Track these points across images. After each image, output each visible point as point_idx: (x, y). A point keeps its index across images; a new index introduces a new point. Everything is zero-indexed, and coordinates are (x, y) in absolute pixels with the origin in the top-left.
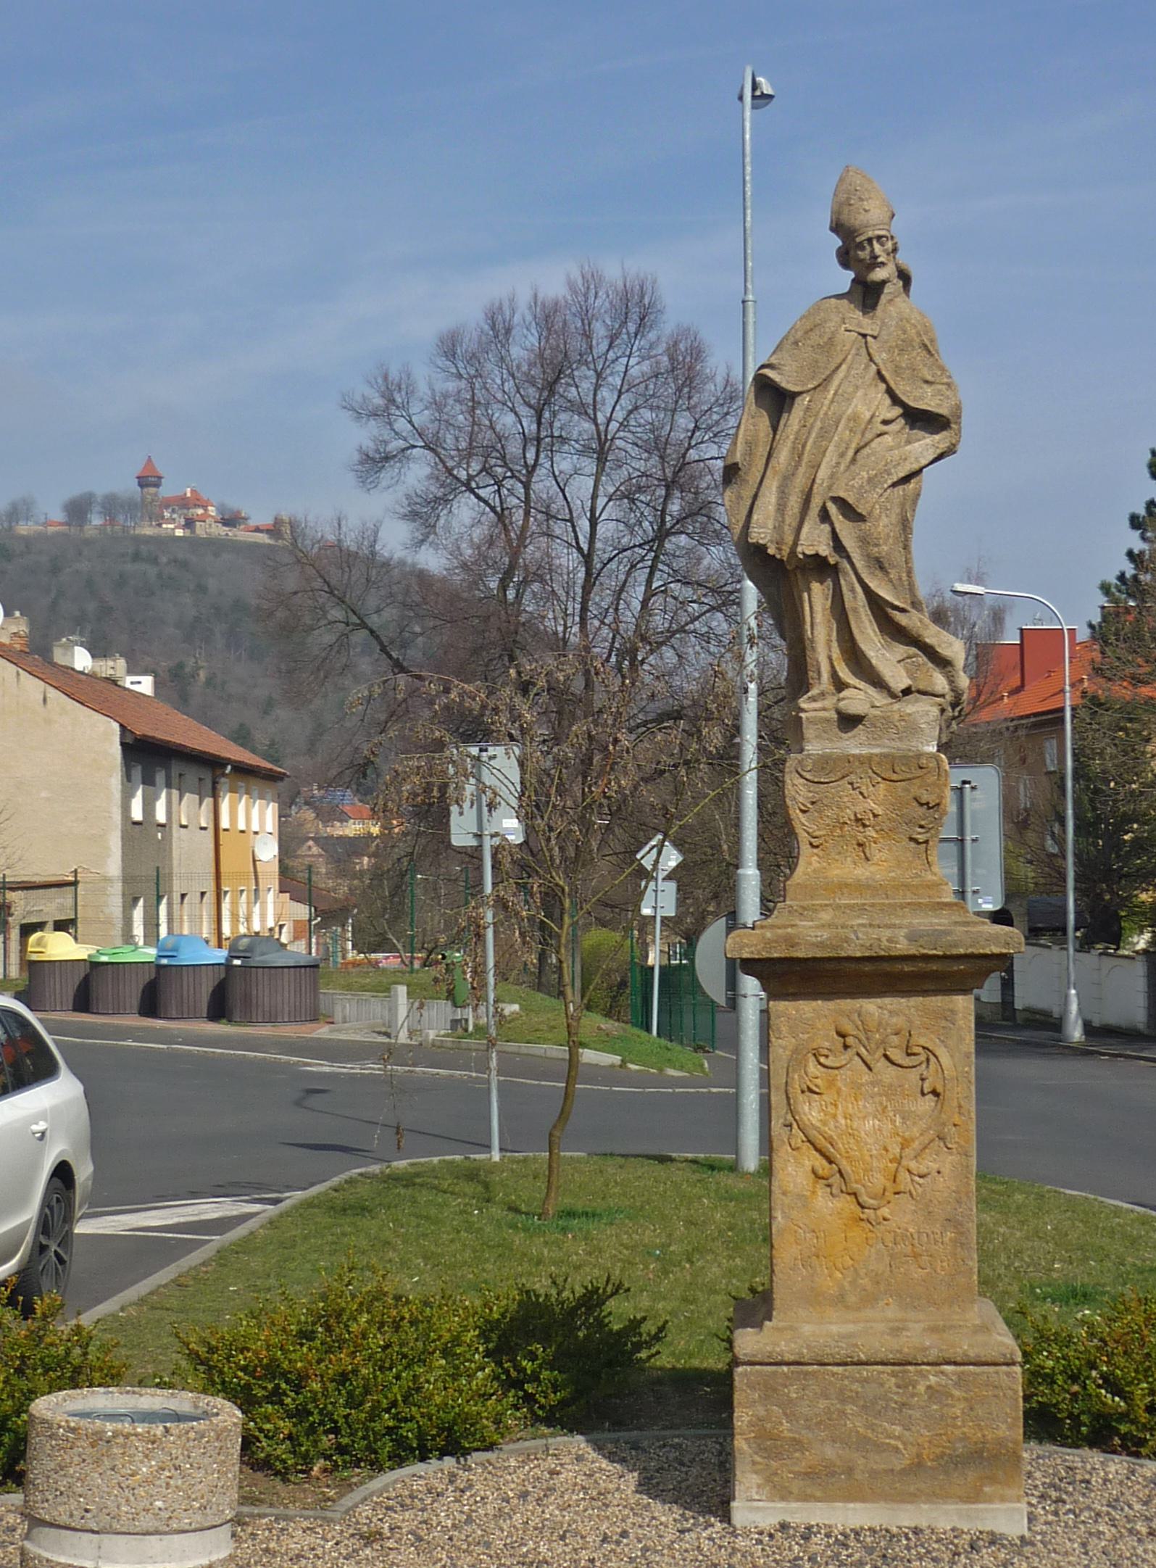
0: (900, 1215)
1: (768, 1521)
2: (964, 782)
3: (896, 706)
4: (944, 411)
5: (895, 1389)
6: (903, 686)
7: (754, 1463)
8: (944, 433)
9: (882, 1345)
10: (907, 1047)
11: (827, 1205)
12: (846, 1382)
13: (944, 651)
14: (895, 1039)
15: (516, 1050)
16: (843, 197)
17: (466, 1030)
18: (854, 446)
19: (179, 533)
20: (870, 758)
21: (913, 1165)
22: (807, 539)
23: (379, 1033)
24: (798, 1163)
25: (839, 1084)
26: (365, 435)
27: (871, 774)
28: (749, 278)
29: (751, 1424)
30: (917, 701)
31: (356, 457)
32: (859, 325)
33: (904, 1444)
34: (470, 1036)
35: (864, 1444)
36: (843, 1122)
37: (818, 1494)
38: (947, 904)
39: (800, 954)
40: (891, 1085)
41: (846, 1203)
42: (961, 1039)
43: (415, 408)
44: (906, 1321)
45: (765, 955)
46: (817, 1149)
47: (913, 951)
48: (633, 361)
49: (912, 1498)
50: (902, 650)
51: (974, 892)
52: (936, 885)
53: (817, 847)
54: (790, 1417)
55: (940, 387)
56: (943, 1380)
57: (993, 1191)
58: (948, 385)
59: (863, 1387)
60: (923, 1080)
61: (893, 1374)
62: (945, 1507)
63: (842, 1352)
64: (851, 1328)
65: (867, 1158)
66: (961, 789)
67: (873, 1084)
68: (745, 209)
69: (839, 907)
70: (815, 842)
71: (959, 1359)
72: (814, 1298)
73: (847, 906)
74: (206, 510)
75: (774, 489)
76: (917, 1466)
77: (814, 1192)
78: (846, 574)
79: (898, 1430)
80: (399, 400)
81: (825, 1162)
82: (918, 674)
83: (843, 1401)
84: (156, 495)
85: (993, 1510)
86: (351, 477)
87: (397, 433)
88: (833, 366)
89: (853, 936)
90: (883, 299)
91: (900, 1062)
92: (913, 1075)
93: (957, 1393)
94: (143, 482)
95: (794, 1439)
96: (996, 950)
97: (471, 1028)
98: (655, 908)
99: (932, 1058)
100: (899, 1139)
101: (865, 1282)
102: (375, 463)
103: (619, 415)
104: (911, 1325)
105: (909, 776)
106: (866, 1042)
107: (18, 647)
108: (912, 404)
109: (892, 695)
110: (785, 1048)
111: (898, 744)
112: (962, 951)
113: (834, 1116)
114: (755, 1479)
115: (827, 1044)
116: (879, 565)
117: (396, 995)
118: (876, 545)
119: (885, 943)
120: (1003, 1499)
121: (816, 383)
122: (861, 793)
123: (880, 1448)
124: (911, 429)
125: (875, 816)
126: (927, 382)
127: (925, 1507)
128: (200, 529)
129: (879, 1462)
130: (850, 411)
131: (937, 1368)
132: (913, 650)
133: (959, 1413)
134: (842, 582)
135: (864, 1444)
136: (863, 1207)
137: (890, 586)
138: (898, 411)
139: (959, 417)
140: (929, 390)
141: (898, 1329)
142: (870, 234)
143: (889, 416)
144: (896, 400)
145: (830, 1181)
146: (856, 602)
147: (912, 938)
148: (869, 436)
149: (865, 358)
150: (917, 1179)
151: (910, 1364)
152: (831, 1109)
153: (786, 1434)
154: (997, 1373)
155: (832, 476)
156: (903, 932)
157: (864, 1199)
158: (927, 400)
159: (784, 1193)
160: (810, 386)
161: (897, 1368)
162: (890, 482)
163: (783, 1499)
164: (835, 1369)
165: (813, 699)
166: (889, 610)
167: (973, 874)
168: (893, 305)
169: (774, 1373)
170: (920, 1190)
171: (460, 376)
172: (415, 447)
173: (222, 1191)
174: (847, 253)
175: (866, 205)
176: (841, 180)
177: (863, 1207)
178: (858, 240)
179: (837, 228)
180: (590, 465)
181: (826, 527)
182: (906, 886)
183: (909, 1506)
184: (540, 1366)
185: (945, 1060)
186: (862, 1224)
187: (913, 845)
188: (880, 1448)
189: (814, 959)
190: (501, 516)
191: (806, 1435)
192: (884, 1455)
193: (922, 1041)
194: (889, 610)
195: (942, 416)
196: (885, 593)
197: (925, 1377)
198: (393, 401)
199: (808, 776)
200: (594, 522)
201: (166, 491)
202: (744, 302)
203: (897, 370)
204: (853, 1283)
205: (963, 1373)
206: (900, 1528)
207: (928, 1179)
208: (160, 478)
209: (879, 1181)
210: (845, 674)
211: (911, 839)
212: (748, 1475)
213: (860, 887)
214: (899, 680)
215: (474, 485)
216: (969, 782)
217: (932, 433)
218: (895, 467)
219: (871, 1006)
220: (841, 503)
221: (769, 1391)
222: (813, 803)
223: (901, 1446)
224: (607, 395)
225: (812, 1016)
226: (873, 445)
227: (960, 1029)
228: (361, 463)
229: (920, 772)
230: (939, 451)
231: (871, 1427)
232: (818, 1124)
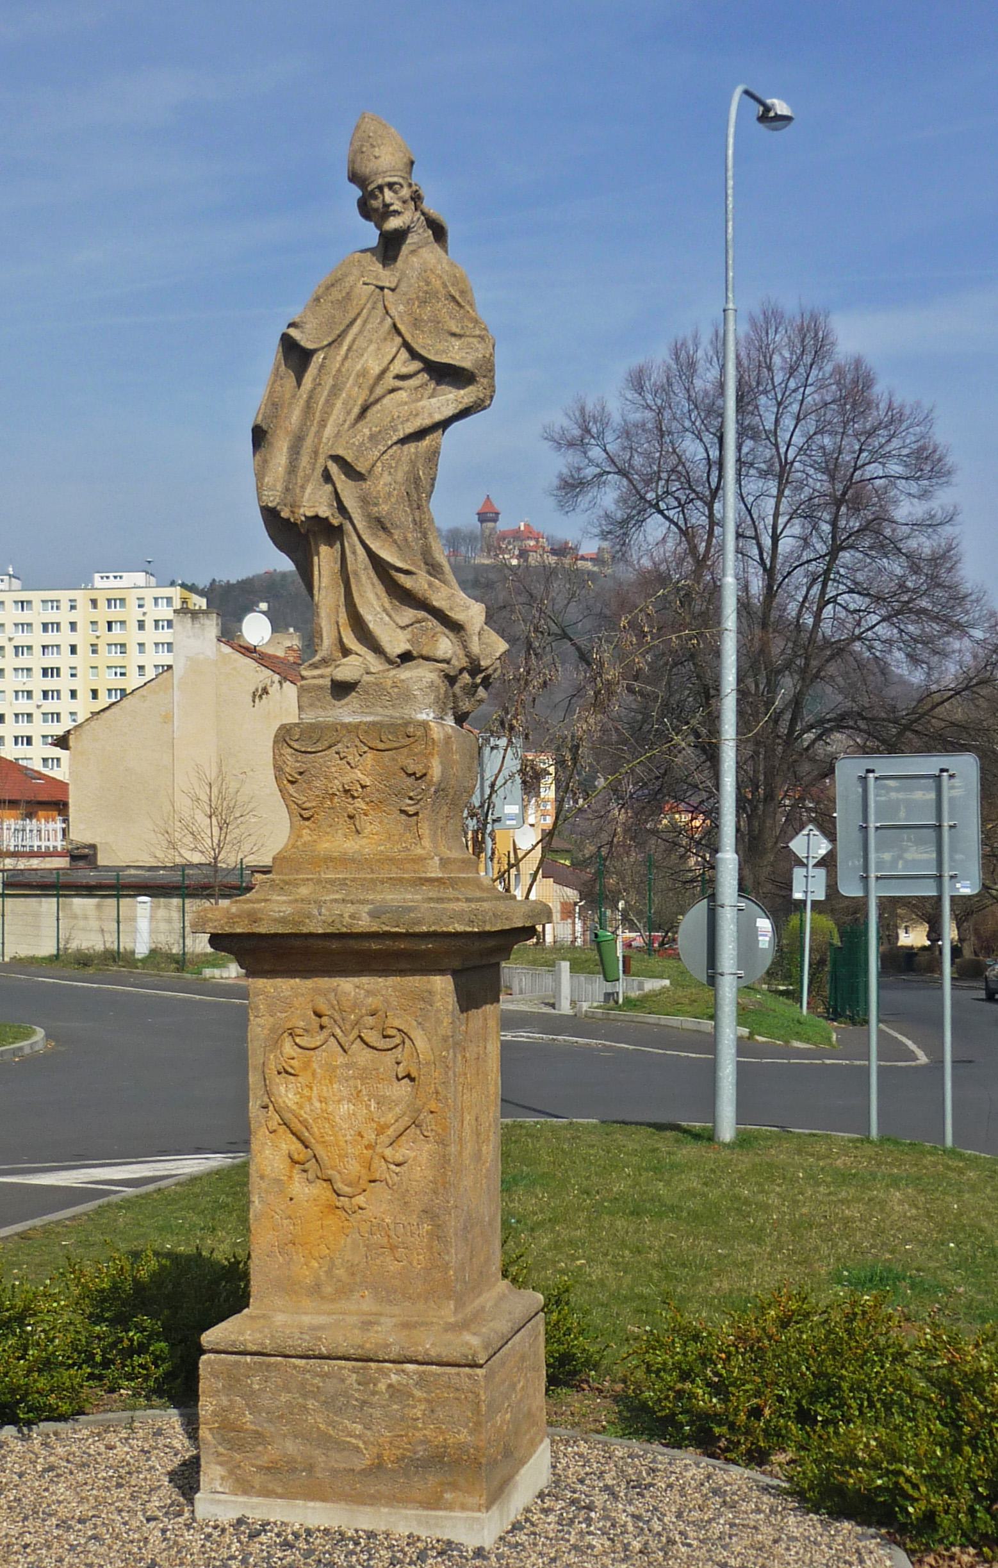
0: (377, 1205)
1: (227, 1515)
2: (942, 770)
3: (393, 673)
4: (467, 364)
5: (356, 1386)
6: (399, 651)
7: (219, 1455)
8: (471, 387)
9: (347, 1339)
10: (384, 1029)
11: (302, 1189)
12: (308, 1376)
13: (457, 616)
14: (370, 1021)
15: (656, 1021)
16: (357, 144)
17: (617, 1002)
18: (360, 402)
19: (514, 562)
20: (357, 726)
21: (388, 1152)
22: (309, 500)
23: (546, 1004)
24: (276, 1146)
25: (315, 1065)
26: (560, 463)
27: (359, 744)
28: (730, 287)
29: (215, 1414)
30: (418, 666)
31: (556, 482)
32: (377, 278)
33: (364, 1443)
34: (620, 1008)
35: (325, 1441)
36: (318, 1105)
37: (280, 1490)
38: (430, 880)
39: (262, 930)
40: (365, 1069)
41: (319, 1190)
42: (439, 1022)
43: (609, 437)
44: (381, 1315)
45: (228, 930)
46: (294, 1134)
47: (374, 929)
48: (809, 390)
49: (372, 1500)
50: (409, 614)
51: (952, 877)
52: (422, 859)
53: (308, 819)
54: (254, 1409)
55: (471, 340)
56: (404, 1379)
57: (948, 1168)
58: (482, 337)
59: (324, 1382)
60: (398, 1063)
61: (353, 1370)
62: (404, 1512)
63: (304, 1344)
64: (322, 1320)
65: (342, 1143)
66: (939, 776)
67: (348, 1066)
68: (727, 221)
69: (319, 881)
70: (306, 814)
71: (420, 1358)
72: (288, 1286)
73: (328, 881)
74: (537, 542)
75: (285, 450)
76: (377, 1468)
77: (290, 1177)
78: (349, 536)
79: (358, 1428)
80: (594, 430)
81: (300, 1146)
82: (424, 640)
83: (305, 1396)
84: (494, 528)
85: (451, 1518)
86: (551, 502)
87: (590, 461)
88: (347, 322)
89: (316, 912)
90: (405, 250)
91: (375, 1045)
92: (389, 1058)
93: (418, 1393)
94: (483, 517)
95: (256, 1432)
96: (460, 928)
97: (621, 1001)
98: (806, 892)
99: (407, 1040)
100: (375, 1126)
101: (340, 1272)
102: (572, 487)
103: (798, 440)
104: (383, 1320)
105: (396, 745)
106: (340, 1022)
107: (291, 659)
108: (432, 357)
109: (390, 661)
110: (262, 1027)
111: (391, 712)
112: (425, 929)
113: (310, 1099)
114: (219, 1471)
115: (302, 1024)
116: (381, 525)
117: (560, 970)
118: (376, 505)
119: (347, 920)
120: (463, 1507)
121: (330, 339)
122: (349, 763)
123: (342, 1447)
124: (438, 384)
125: (363, 787)
126: (454, 335)
127: (385, 1510)
128: (533, 559)
129: (338, 1460)
130: (359, 367)
131: (399, 1366)
132: (422, 614)
133: (419, 1414)
134: (346, 544)
135: (325, 1441)
136: (339, 1195)
137: (394, 549)
138: (416, 365)
139: (492, 370)
140: (457, 343)
141: (371, 1323)
142: (380, 181)
143: (404, 370)
144: (414, 355)
145: (307, 1166)
146: (359, 561)
147: (374, 915)
148: (379, 391)
149: (380, 311)
150: (393, 1167)
151: (371, 1360)
152: (306, 1092)
153: (249, 1426)
154: (458, 1374)
155: (338, 435)
156: (368, 908)
157: (339, 1185)
158: (456, 354)
159: (262, 1177)
160: (325, 343)
161: (360, 1364)
162: (395, 439)
163: (245, 1493)
164: (301, 1362)
165: (315, 666)
166: (393, 573)
167: (952, 859)
168: (420, 256)
169: (237, 1363)
170: (396, 1179)
171: (648, 407)
172: (609, 473)
173: (233, 1147)
174: (365, 204)
175: (377, 152)
176: (357, 127)
177: (339, 1195)
178: (369, 189)
179: (355, 178)
180: (772, 486)
181: (329, 487)
182: (391, 860)
183: (368, 1509)
184: (150, 1337)
185: (421, 1042)
186: (338, 1212)
187: (404, 817)
188: (342, 1447)
189: (276, 935)
190: (686, 533)
191: (268, 1428)
192: (346, 1453)
193: (397, 1023)
194: (393, 573)
195: (463, 369)
196: (388, 555)
197: (387, 1375)
198: (588, 431)
199: (296, 746)
200: (775, 539)
201: (503, 525)
202: (724, 311)
203: (416, 323)
204: (329, 1273)
205: (424, 1372)
206: (357, 1531)
207: (404, 1168)
209: (354, 1168)
210: (351, 641)
211: (402, 812)
212: (213, 1466)
213: (344, 860)
214: (396, 642)
215: (662, 506)
216: (947, 771)
217: (459, 388)
218: (402, 423)
219: (347, 985)
220: (337, 459)
221: (233, 1382)
222: (301, 773)
223: (361, 1445)
224: (788, 422)
225: (283, 996)
226: (385, 401)
227: (438, 1011)
228: (559, 488)
229: (407, 741)
230: (461, 407)
231: (331, 1424)
232: (294, 1107)
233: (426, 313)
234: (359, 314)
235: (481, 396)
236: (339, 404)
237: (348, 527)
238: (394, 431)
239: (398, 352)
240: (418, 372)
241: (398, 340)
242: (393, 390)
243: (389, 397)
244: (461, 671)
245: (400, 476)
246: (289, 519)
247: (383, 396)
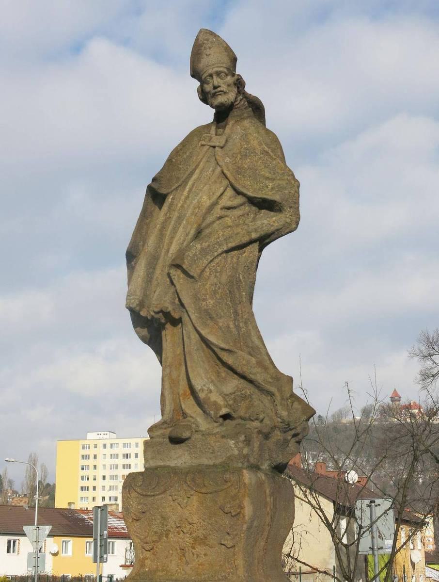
31: (419, 376)
116: (208, 315)
118: (204, 300)
138: (240, 200)
142: (210, 71)
143: (229, 204)
144: (238, 193)
148: (210, 219)
162: (220, 251)
181: (172, 289)
208: (400, 397)
226: (215, 225)
233: (247, 163)
234: (197, 166)
235: (288, 220)
236: (181, 229)
237: (185, 318)
238: (220, 246)
239: (225, 190)
240: (241, 205)
241: (225, 182)
242: (220, 218)
243: (218, 222)
244: (274, 428)
245: (224, 278)
246: (147, 317)
247: (214, 222)
